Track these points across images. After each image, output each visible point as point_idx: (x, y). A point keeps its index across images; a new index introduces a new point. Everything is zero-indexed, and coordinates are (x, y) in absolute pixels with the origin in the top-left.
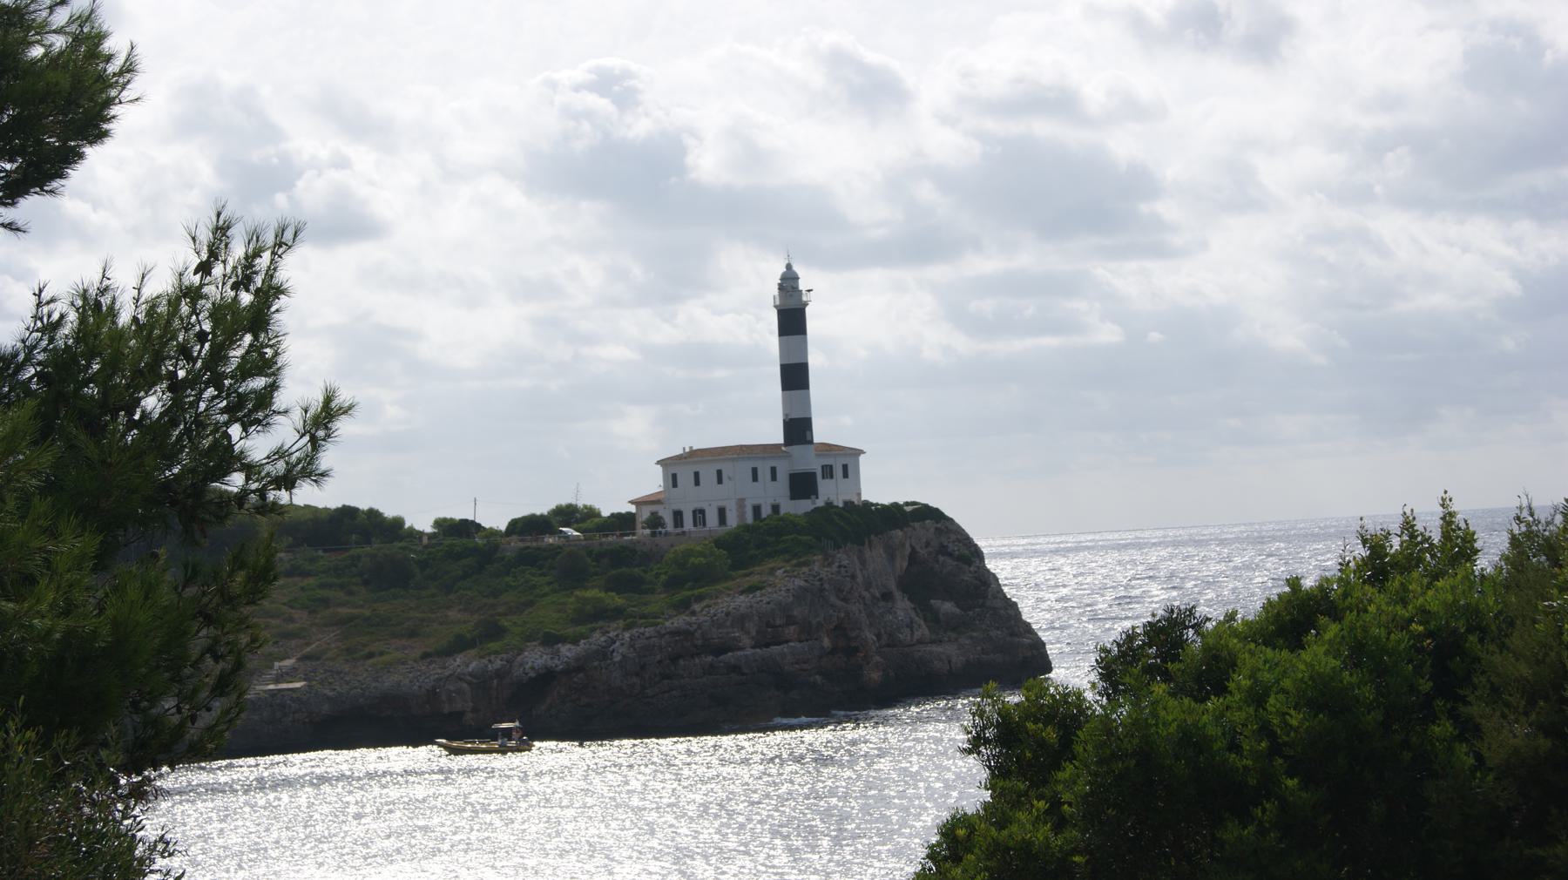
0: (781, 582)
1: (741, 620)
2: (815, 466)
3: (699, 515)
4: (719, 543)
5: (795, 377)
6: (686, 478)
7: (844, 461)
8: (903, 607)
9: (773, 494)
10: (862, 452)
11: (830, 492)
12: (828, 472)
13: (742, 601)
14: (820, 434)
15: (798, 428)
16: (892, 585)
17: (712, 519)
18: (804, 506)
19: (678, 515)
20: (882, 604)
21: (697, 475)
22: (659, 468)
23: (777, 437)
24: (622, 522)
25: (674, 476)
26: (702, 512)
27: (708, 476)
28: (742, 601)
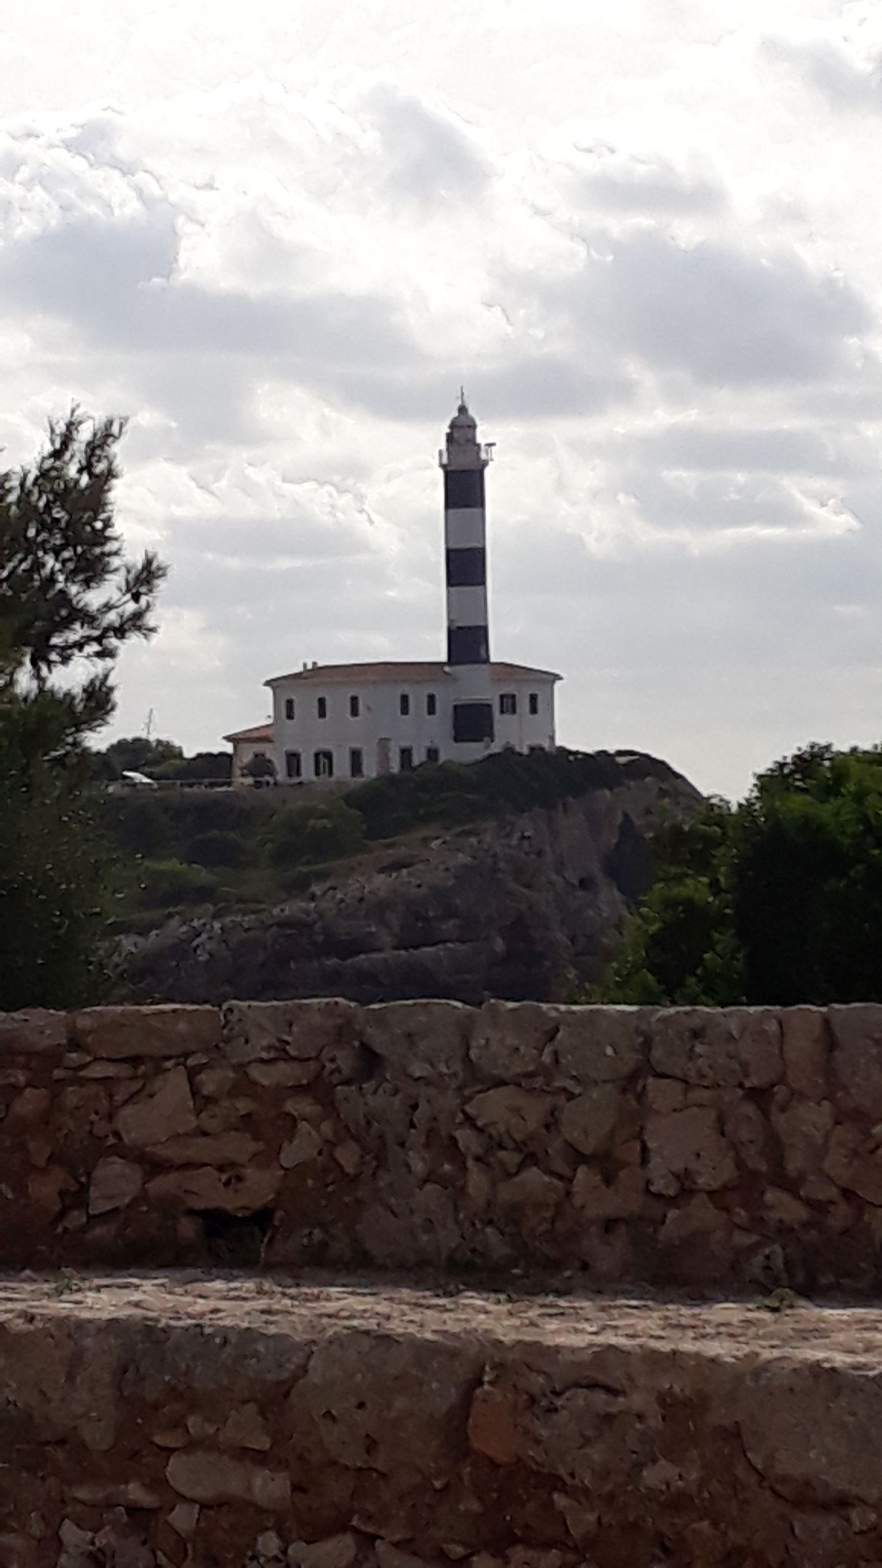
0: (436, 858)
1: (379, 909)
2: (490, 695)
3: (323, 760)
4: (352, 799)
5: (465, 567)
6: (305, 706)
7: (532, 689)
9: (426, 733)
10: (557, 677)
11: (511, 733)
12: (509, 704)
13: (381, 882)
14: (499, 650)
15: (467, 640)
16: (595, 868)
17: (342, 767)
18: (474, 751)
19: (293, 759)
20: (580, 893)
21: (322, 702)
22: (269, 691)
23: (435, 648)
24: (213, 765)
25: (290, 703)
26: (328, 755)
27: (338, 702)
28: (381, 882)
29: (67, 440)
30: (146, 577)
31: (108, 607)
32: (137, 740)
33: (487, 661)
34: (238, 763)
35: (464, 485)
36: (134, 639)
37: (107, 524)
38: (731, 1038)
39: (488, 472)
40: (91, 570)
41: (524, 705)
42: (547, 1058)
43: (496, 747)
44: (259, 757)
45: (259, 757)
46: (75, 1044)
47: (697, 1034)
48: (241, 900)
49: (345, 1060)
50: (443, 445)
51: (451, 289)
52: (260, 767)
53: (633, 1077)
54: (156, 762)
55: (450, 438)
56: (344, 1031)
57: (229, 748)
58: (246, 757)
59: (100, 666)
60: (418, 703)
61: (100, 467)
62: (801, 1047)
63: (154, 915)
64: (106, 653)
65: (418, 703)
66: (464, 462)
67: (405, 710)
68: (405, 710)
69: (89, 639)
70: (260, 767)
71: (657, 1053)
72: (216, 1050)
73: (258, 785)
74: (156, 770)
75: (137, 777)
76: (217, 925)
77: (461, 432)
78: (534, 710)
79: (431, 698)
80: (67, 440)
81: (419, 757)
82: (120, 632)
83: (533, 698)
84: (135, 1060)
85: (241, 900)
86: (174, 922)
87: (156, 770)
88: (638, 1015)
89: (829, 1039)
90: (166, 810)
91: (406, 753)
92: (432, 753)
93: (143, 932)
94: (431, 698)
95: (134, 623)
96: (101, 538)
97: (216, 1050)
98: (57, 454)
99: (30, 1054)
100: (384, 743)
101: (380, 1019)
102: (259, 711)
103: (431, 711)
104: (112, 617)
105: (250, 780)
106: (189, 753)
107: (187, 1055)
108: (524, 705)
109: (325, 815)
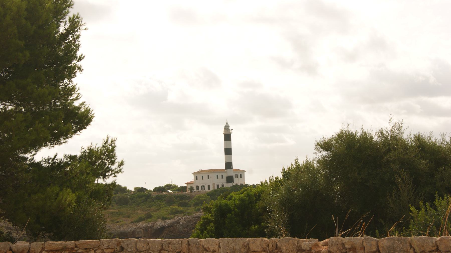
3: (203, 187)
4: (208, 194)
5: (228, 152)
6: (200, 177)
7: (240, 174)
9: (222, 182)
10: (245, 171)
11: (237, 181)
12: (236, 176)
14: (234, 167)
15: (229, 165)
17: (206, 188)
18: (230, 185)
19: (197, 187)
21: (202, 177)
22: (193, 175)
24: (183, 189)
25: (197, 177)
26: (204, 186)
29: (107, 141)
30: (121, 164)
31: (115, 169)
32: (142, 188)
33: (232, 168)
34: (188, 188)
35: (228, 137)
36: (120, 174)
37: (115, 154)
38: (174, 244)
39: (232, 135)
40: (113, 163)
41: (239, 176)
42: (148, 248)
43: (234, 184)
44: (191, 187)
45: (191, 187)
46: (76, 247)
47: (169, 243)
48: (188, 213)
49: (118, 248)
50: (224, 130)
51: (222, 103)
52: (192, 189)
53: (161, 250)
54: (173, 188)
55: (225, 129)
56: (119, 244)
57: (186, 185)
58: (189, 187)
59: (115, 178)
60: (220, 176)
61: (113, 145)
62: (184, 245)
63: (172, 216)
64: (115, 176)
65: (220, 176)
66: (227, 133)
67: (217, 178)
68: (217, 178)
69: (112, 174)
70: (192, 189)
71: (164, 247)
72: (99, 247)
73: (191, 192)
74: (173, 189)
75: (169, 191)
76: (184, 218)
77: (227, 128)
78: (241, 177)
79: (222, 176)
80: (107, 141)
81: (220, 186)
82: (118, 172)
83: (241, 175)
84: (86, 249)
85: (188, 213)
86: (176, 217)
87: (173, 189)
88: (161, 241)
89: (189, 244)
90: (175, 197)
91: (218, 186)
92: (223, 186)
93: (170, 219)
94: (222, 176)
95: (120, 171)
96: (113, 157)
97: (99, 247)
98: (106, 143)
99: (69, 248)
100: (214, 184)
101: (123, 242)
102: (191, 178)
103: (222, 178)
104: (116, 170)
105: (190, 191)
106: (179, 186)
107: (94, 248)
108: (239, 176)
109: (203, 197)
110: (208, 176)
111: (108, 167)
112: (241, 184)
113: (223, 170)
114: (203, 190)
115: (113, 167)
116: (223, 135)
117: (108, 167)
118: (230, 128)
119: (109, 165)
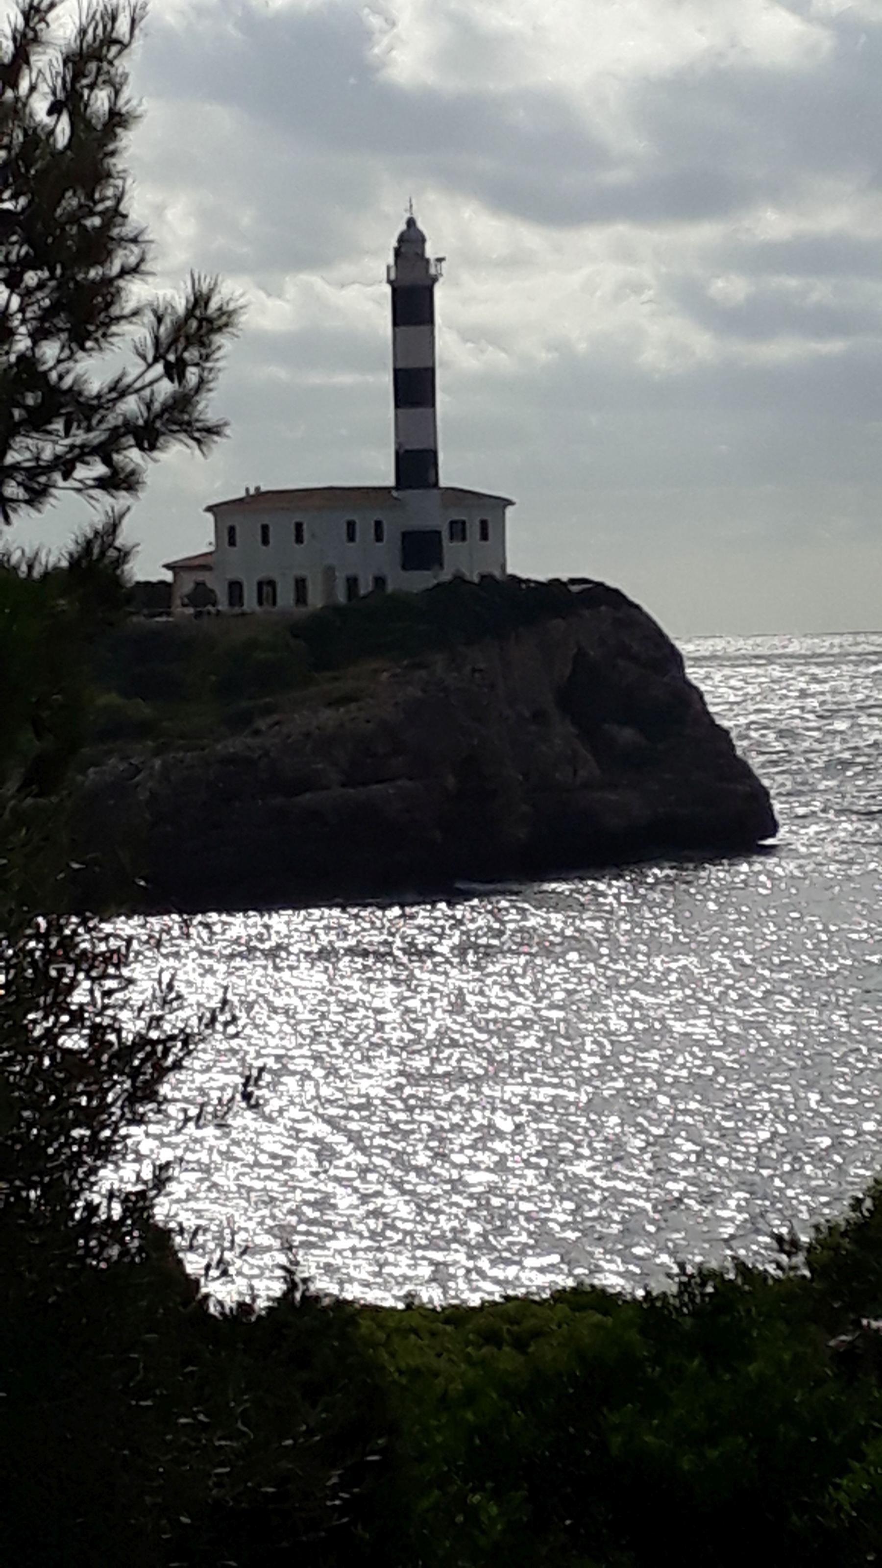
0: (381, 691)
3: (267, 589)
4: (297, 630)
5: (414, 387)
7: (483, 514)
8: (562, 732)
9: (373, 561)
10: (510, 503)
11: (460, 560)
12: (458, 530)
13: (328, 717)
14: (452, 473)
15: (416, 464)
17: (286, 596)
18: (420, 581)
19: (235, 589)
21: (265, 529)
22: (210, 517)
23: (383, 473)
25: (232, 530)
26: (272, 583)
27: (282, 528)
28: (328, 717)
33: (436, 484)
35: (412, 301)
36: (176, 452)
37: (115, 215)
41: (473, 530)
43: (446, 576)
44: (199, 585)
45: (199, 585)
50: (391, 260)
52: (201, 596)
57: (168, 576)
58: (187, 586)
59: (106, 503)
64: (119, 481)
69: (82, 454)
70: (201, 596)
73: (198, 615)
76: (158, 763)
78: (484, 536)
81: (365, 587)
82: (148, 436)
83: (484, 524)
91: (352, 583)
92: (380, 581)
96: (100, 245)
100: (329, 572)
105: (191, 611)
108: (473, 530)
110: (299, 527)
111: (27, 361)
112: (483, 577)
113: (387, 489)
114: (267, 607)
115: (94, 371)
116: (387, 289)
117: (27, 361)
118: (430, 252)
119: (38, 336)
